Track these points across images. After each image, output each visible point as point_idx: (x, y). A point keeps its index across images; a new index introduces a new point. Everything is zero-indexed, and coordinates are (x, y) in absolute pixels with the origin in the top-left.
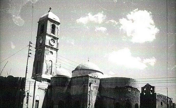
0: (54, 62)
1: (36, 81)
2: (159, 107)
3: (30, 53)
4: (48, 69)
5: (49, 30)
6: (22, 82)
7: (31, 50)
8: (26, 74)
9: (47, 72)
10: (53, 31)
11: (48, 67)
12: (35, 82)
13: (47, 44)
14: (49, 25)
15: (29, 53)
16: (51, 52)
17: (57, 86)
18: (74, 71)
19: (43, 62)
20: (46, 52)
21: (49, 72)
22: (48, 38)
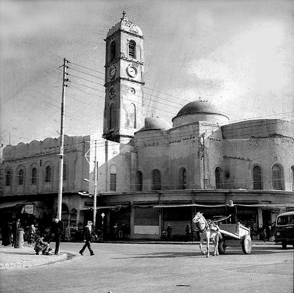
0: (139, 106)
1: (109, 141)
2: (293, 201)
3: (67, 80)
4: (129, 118)
5: (124, 49)
6: (85, 143)
7: (67, 74)
8: (62, 118)
9: (128, 124)
10: (133, 54)
11: (129, 115)
12: (106, 142)
13: (123, 74)
14: (124, 40)
15: (64, 80)
16: (133, 90)
17: (145, 145)
18: (175, 117)
19: (119, 108)
20: (122, 89)
21: (132, 124)
22: (124, 65)
